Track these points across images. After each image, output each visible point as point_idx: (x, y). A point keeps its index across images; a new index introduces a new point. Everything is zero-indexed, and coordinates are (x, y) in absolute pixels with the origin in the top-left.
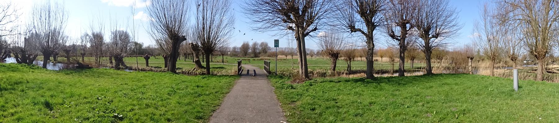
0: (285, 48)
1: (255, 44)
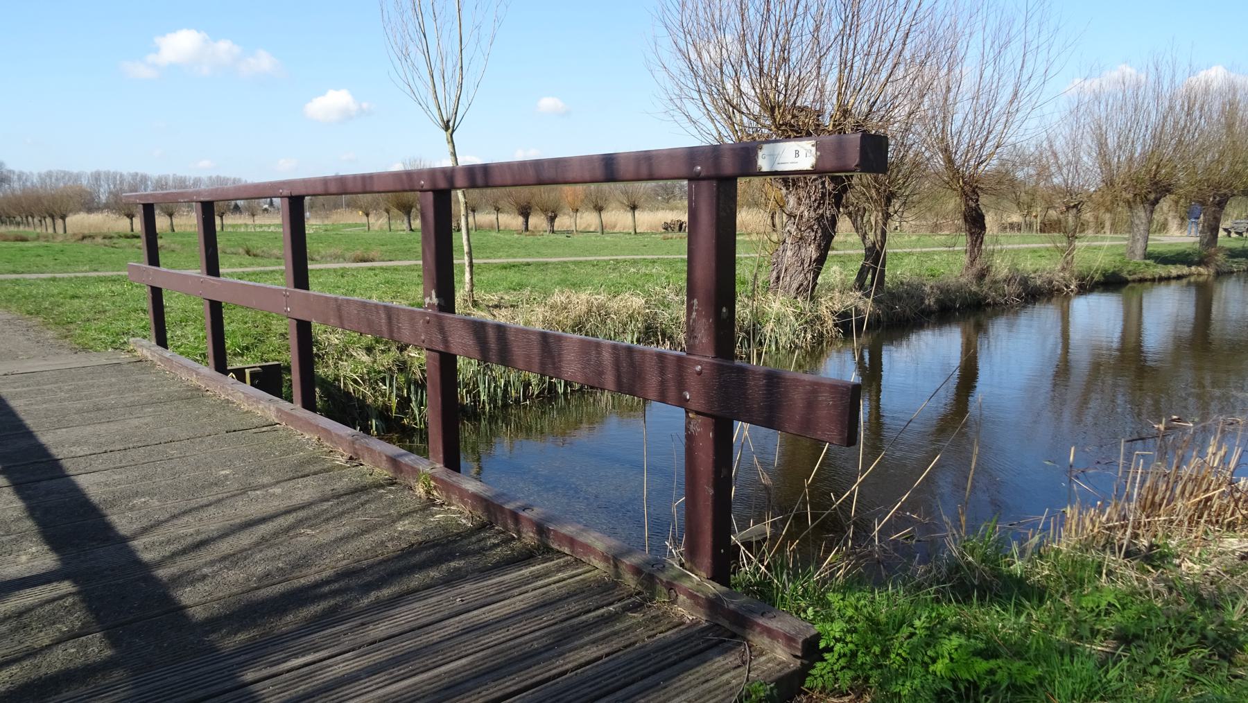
0: (97, 177)
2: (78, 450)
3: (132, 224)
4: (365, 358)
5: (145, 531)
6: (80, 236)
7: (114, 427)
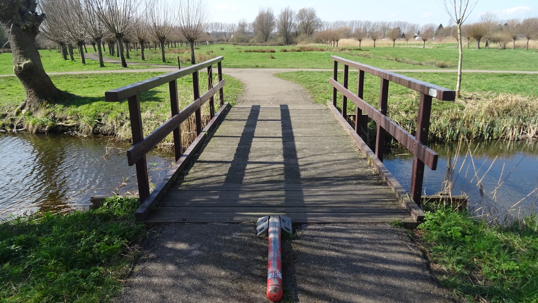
0: (352, 23)
1: (286, 15)
2: (299, 135)
4: (404, 115)
5: (302, 158)
6: (341, 49)
7: (310, 130)
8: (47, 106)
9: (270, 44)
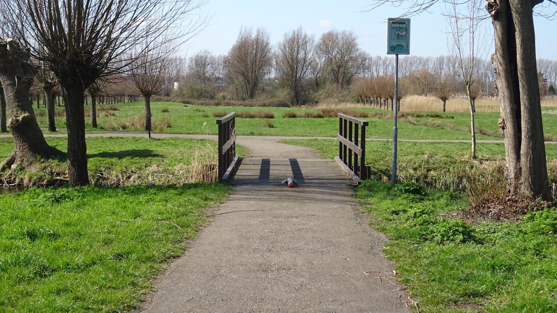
0: (441, 61)
3: (445, 105)
4: (412, 171)
8: (42, 160)
9: (262, 103)
